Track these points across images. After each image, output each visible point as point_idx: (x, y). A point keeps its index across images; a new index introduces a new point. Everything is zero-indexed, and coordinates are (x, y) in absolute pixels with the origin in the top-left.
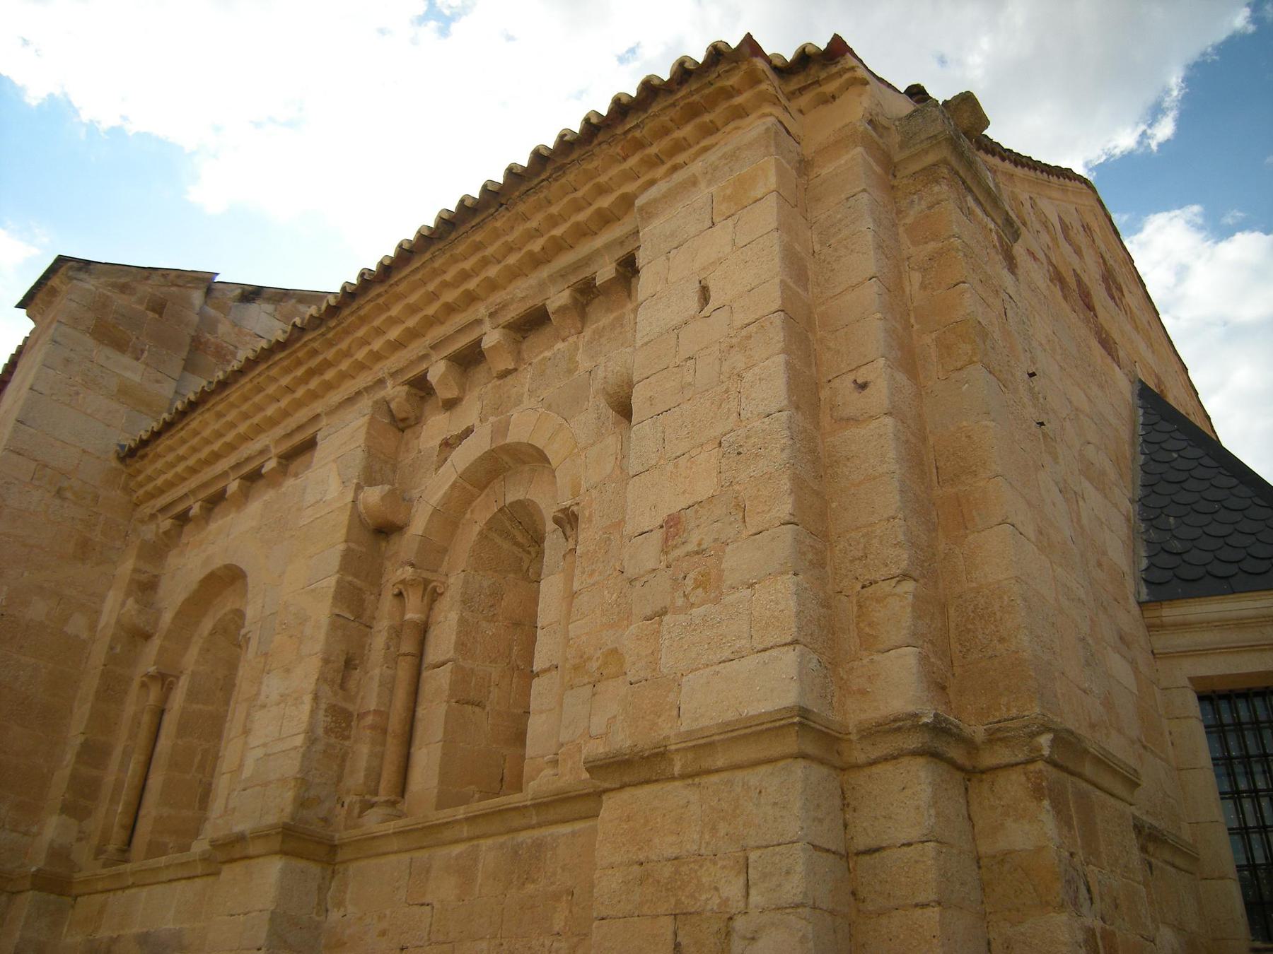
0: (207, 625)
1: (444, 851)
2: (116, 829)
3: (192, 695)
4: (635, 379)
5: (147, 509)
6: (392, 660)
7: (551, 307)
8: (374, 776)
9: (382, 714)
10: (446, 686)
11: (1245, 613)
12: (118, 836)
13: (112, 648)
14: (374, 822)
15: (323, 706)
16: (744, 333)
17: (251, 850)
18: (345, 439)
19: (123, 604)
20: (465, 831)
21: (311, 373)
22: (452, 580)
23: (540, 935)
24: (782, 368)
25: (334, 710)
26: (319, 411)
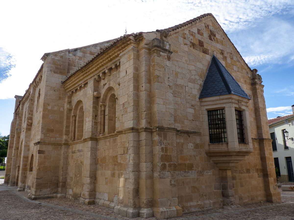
0: (79, 108)
1: (107, 139)
2: (72, 136)
3: (79, 118)
5: (67, 91)
6: (101, 115)
8: (101, 130)
9: (101, 122)
11: (213, 99)
12: (73, 137)
13: (67, 112)
14: (101, 136)
15: (93, 122)
17: (88, 140)
18: (91, 84)
20: (109, 137)
21: (85, 74)
22: (107, 104)
25: (95, 122)
26: (87, 79)
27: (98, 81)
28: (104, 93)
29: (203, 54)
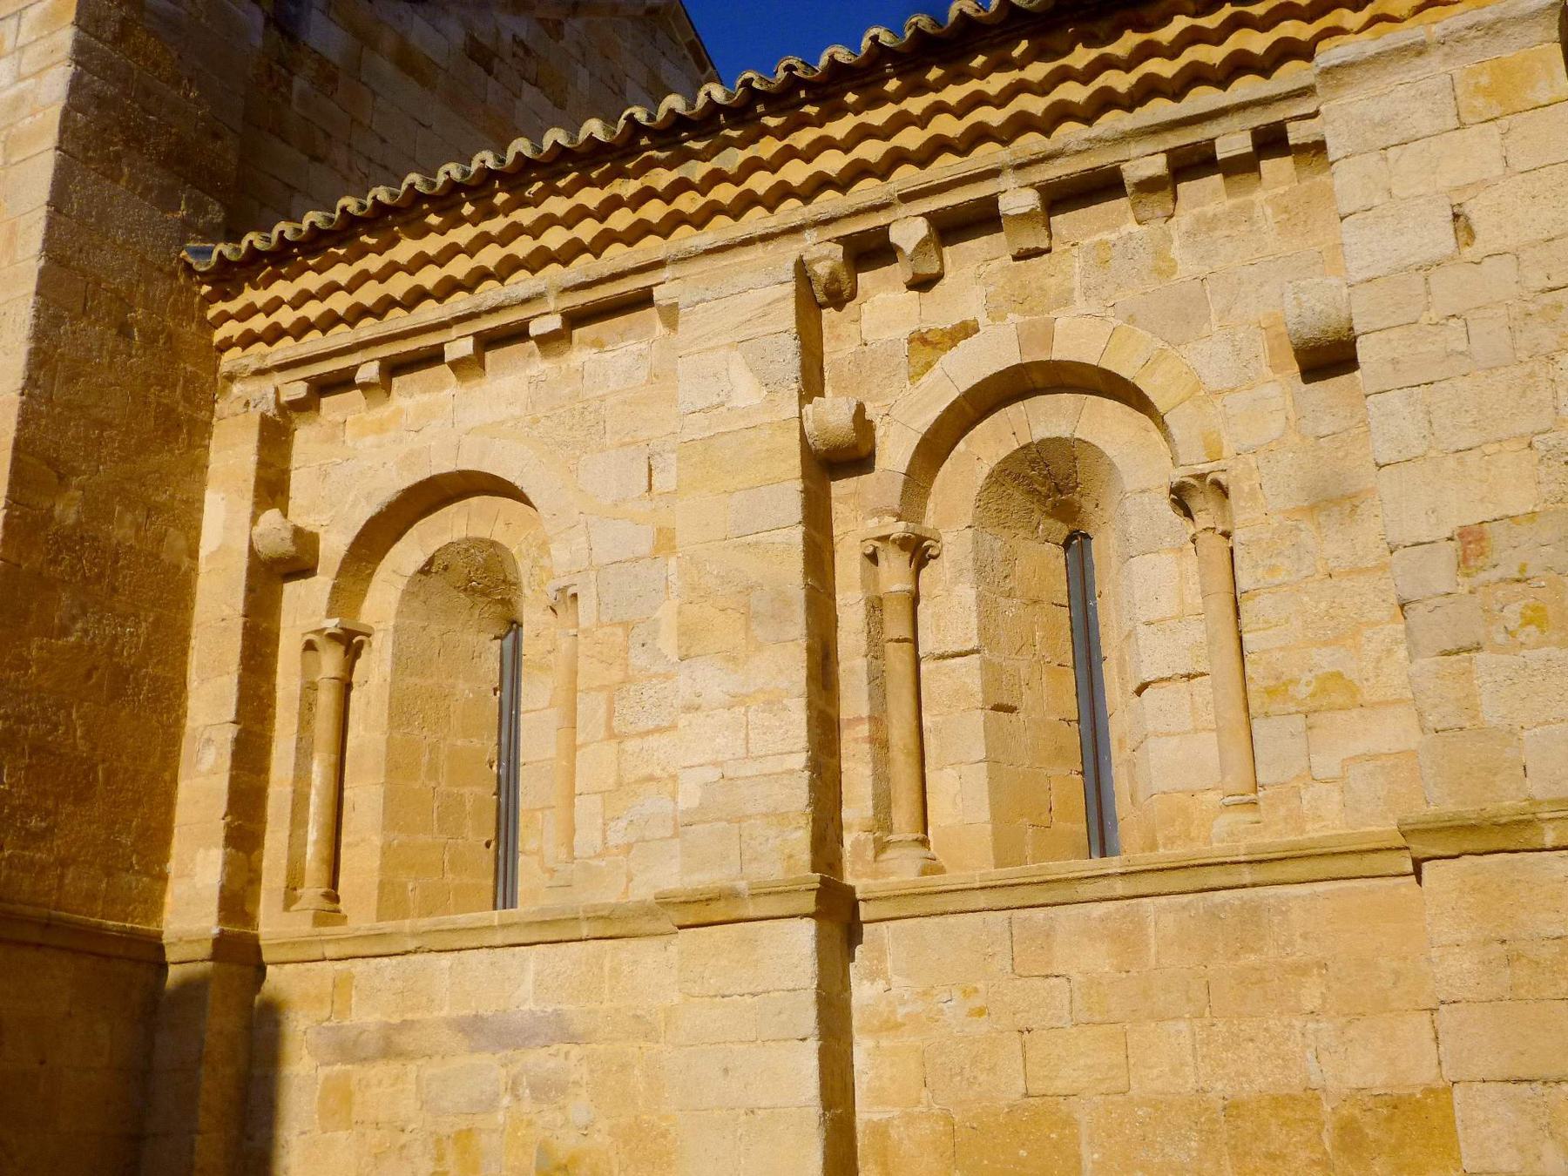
3: (401, 662)
4: (1358, 329)
16: (1548, 298)
19: (254, 519)
23: (1281, 1013)
28: (197, 529)
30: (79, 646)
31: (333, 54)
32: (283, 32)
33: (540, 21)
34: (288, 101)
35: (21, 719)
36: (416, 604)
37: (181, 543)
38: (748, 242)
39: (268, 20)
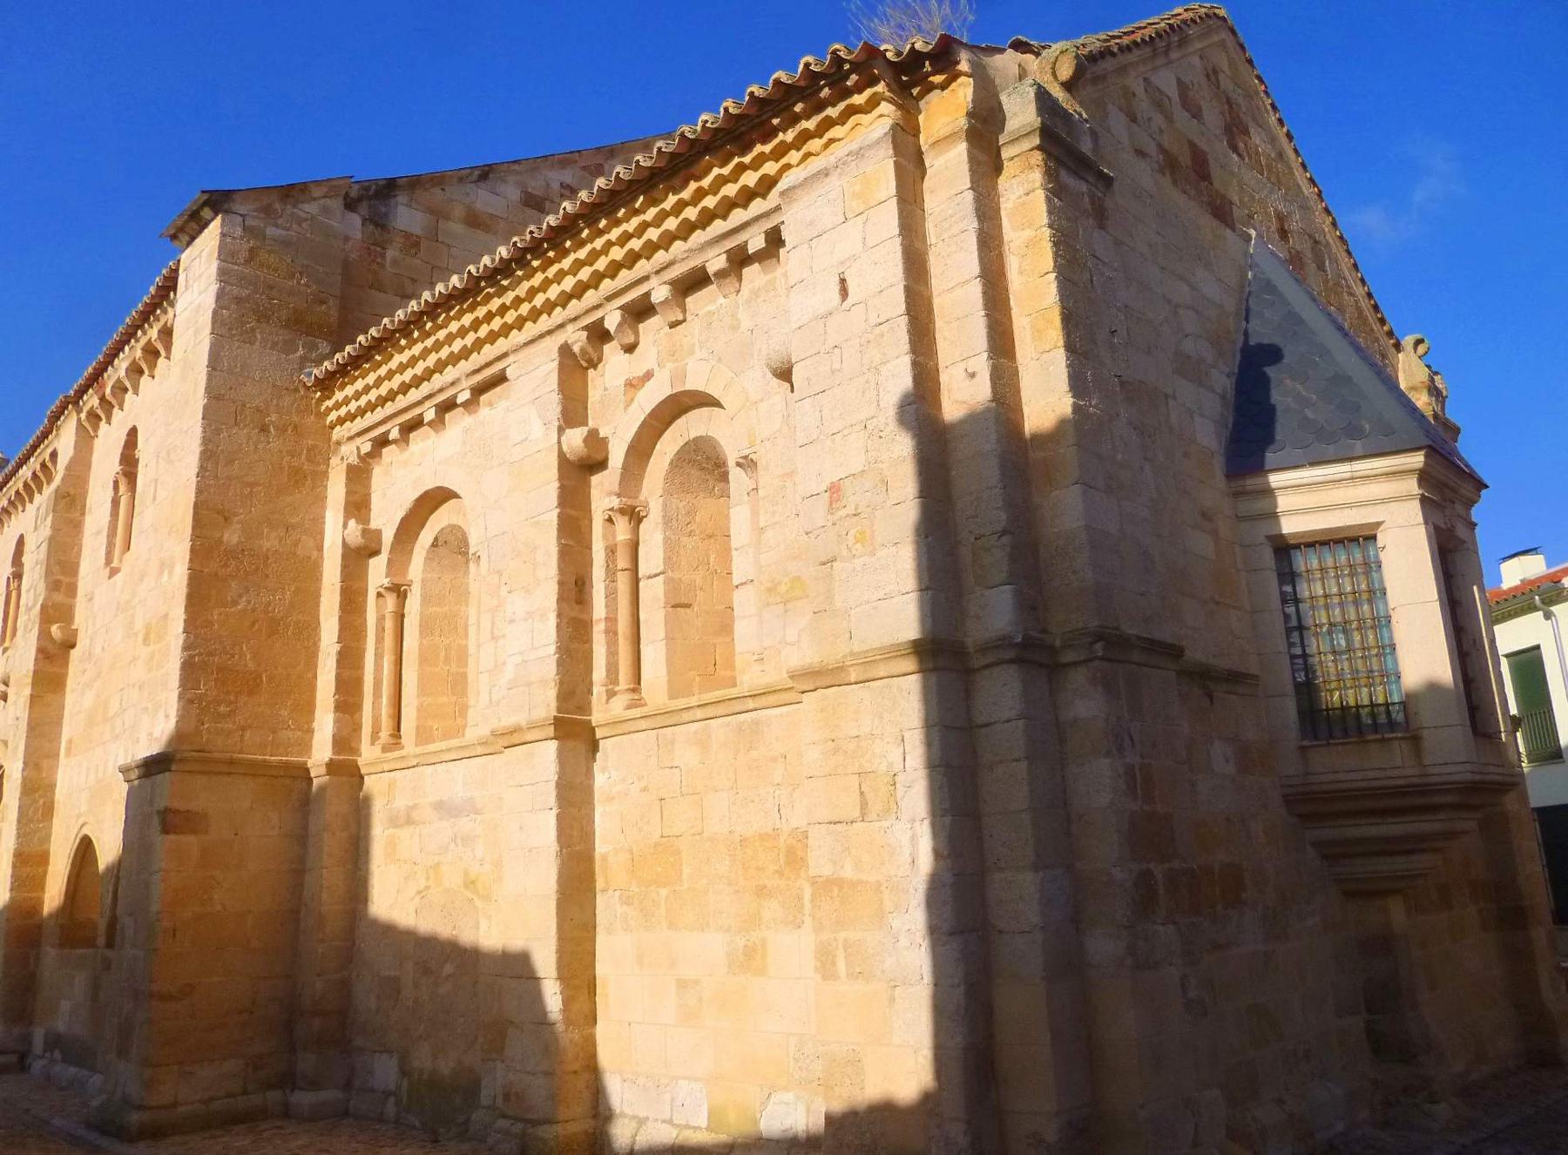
3: (426, 600)
7: (712, 268)
10: (661, 595)
16: (878, 330)
18: (534, 373)
19: (345, 526)
24: (909, 367)
27: (575, 369)
28: (322, 533)
29: (1216, 223)
30: (245, 610)
31: (417, 230)
32: (377, 225)
33: (584, 168)
34: (383, 266)
35: (211, 654)
36: (434, 564)
37: (311, 544)
38: (542, 336)
39: (364, 220)
